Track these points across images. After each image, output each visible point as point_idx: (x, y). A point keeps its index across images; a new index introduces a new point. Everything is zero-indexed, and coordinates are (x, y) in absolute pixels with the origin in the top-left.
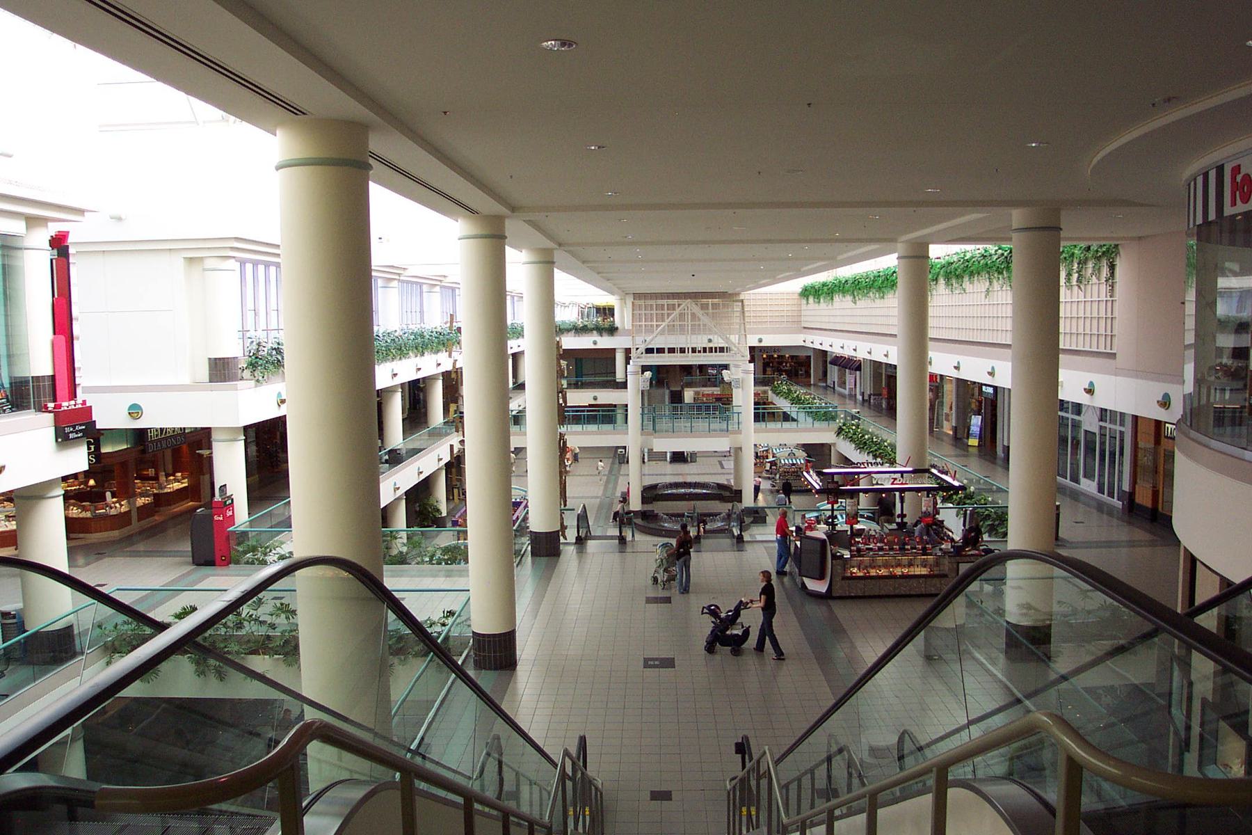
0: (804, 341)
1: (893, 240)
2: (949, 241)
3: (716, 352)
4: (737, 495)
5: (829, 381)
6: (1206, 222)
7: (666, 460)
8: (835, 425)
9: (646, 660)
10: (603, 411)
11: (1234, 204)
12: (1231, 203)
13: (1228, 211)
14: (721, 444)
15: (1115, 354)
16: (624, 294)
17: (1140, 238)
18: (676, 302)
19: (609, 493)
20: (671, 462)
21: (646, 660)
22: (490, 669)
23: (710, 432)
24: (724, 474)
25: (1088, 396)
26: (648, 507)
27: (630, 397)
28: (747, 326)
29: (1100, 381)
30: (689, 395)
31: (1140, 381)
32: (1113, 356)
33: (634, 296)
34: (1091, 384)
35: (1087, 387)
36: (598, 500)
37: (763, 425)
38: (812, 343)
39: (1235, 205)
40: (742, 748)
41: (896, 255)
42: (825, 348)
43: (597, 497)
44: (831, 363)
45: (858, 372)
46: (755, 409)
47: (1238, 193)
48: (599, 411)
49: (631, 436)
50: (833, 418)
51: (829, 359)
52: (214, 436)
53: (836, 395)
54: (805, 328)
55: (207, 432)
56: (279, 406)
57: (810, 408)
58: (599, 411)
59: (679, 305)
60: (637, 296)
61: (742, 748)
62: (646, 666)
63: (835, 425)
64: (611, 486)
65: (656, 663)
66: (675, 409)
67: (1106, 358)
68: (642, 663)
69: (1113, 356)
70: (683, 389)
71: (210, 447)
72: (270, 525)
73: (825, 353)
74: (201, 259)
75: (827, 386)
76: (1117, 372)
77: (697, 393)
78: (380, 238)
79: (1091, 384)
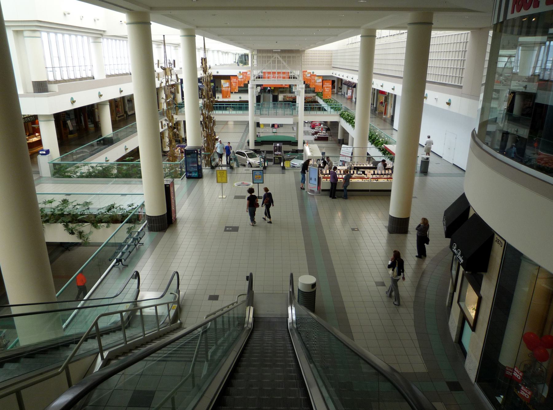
0: (333, 73)
1: (359, 27)
2: (386, 28)
3: (291, 78)
4: (296, 144)
5: (342, 92)
6: (498, 23)
7: (270, 126)
8: (339, 113)
9: (226, 227)
10: (239, 105)
11: (513, 12)
12: (512, 12)
13: (510, 16)
14: (289, 121)
15: (462, 86)
16: (252, 50)
17: (480, 29)
18: (270, 55)
19: (243, 141)
20: (272, 127)
21: (226, 227)
22: (154, 231)
23: (284, 115)
24: (293, 133)
25: (448, 106)
26: (258, 148)
27: (250, 97)
28: (303, 66)
29: (455, 99)
30: (281, 97)
31: (471, 100)
32: (461, 87)
33: (257, 51)
34: (450, 100)
35: (448, 102)
36: (238, 144)
37: (308, 112)
38: (336, 74)
39: (513, 13)
40: (250, 278)
41: (360, 35)
42: (341, 77)
43: (237, 143)
44: (344, 84)
45: (354, 88)
46: (305, 105)
47: (516, 5)
48: (237, 105)
49: (250, 116)
50: (339, 110)
51: (343, 82)
52: (40, 119)
53: (345, 99)
54: (333, 67)
55: (36, 117)
56: (72, 104)
57: (336, 105)
58: (237, 105)
59: (273, 56)
60: (259, 51)
61: (250, 278)
62: (225, 230)
63: (339, 113)
64: (244, 137)
65: (231, 229)
66: (274, 104)
67: (459, 88)
68: (224, 229)
69: (461, 87)
70: (278, 94)
71: (38, 124)
72: (72, 160)
73: (342, 80)
74: (22, 31)
75: (342, 94)
76: (462, 95)
77: (285, 96)
78: (121, 21)
79: (450, 100)
